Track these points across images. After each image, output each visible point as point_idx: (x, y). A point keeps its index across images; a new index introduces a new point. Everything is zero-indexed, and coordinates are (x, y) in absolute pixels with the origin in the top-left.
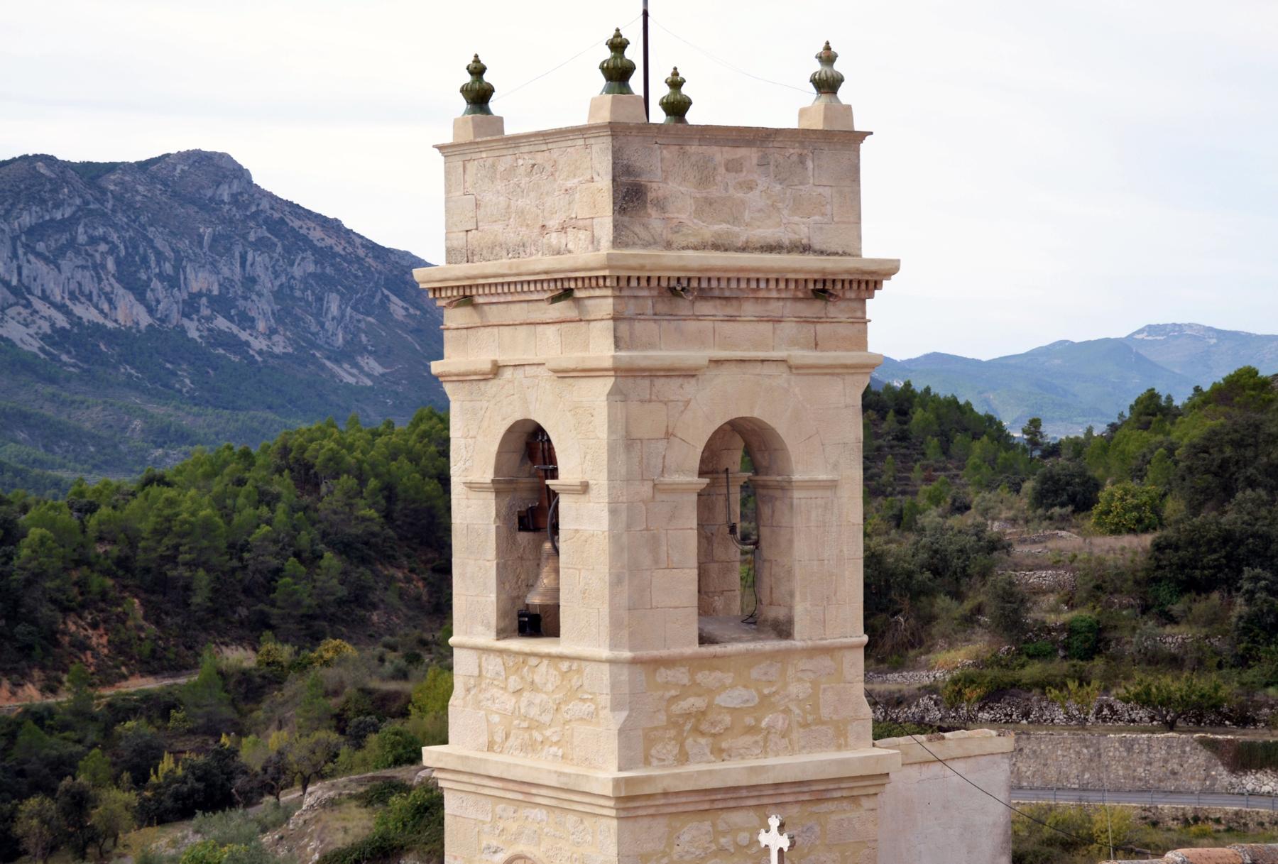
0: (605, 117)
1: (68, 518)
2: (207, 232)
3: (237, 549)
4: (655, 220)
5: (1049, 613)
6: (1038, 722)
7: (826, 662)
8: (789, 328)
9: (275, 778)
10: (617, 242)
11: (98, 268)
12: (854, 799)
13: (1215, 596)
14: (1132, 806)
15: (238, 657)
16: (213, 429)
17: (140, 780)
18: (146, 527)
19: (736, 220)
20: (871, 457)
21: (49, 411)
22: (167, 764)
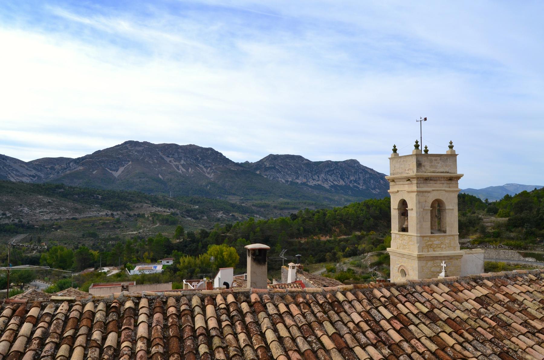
0: (415, 153)
1: (333, 213)
2: (353, 171)
3: (358, 217)
4: (423, 169)
5: (490, 230)
6: (488, 248)
7: (452, 237)
8: (445, 185)
9: (364, 251)
10: (417, 171)
11: (337, 176)
12: (457, 259)
13: (520, 228)
14: (505, 262)
15: (358, 233)
16: (354, 200)
17: (343, 251)
18: (344, 214)
19: (436, 168)
20: (459, 204)
21: (330, 197)
22: (347, 249)
